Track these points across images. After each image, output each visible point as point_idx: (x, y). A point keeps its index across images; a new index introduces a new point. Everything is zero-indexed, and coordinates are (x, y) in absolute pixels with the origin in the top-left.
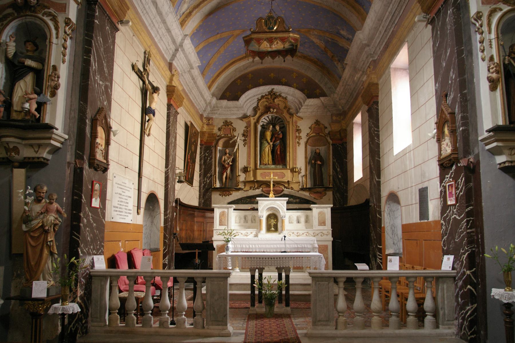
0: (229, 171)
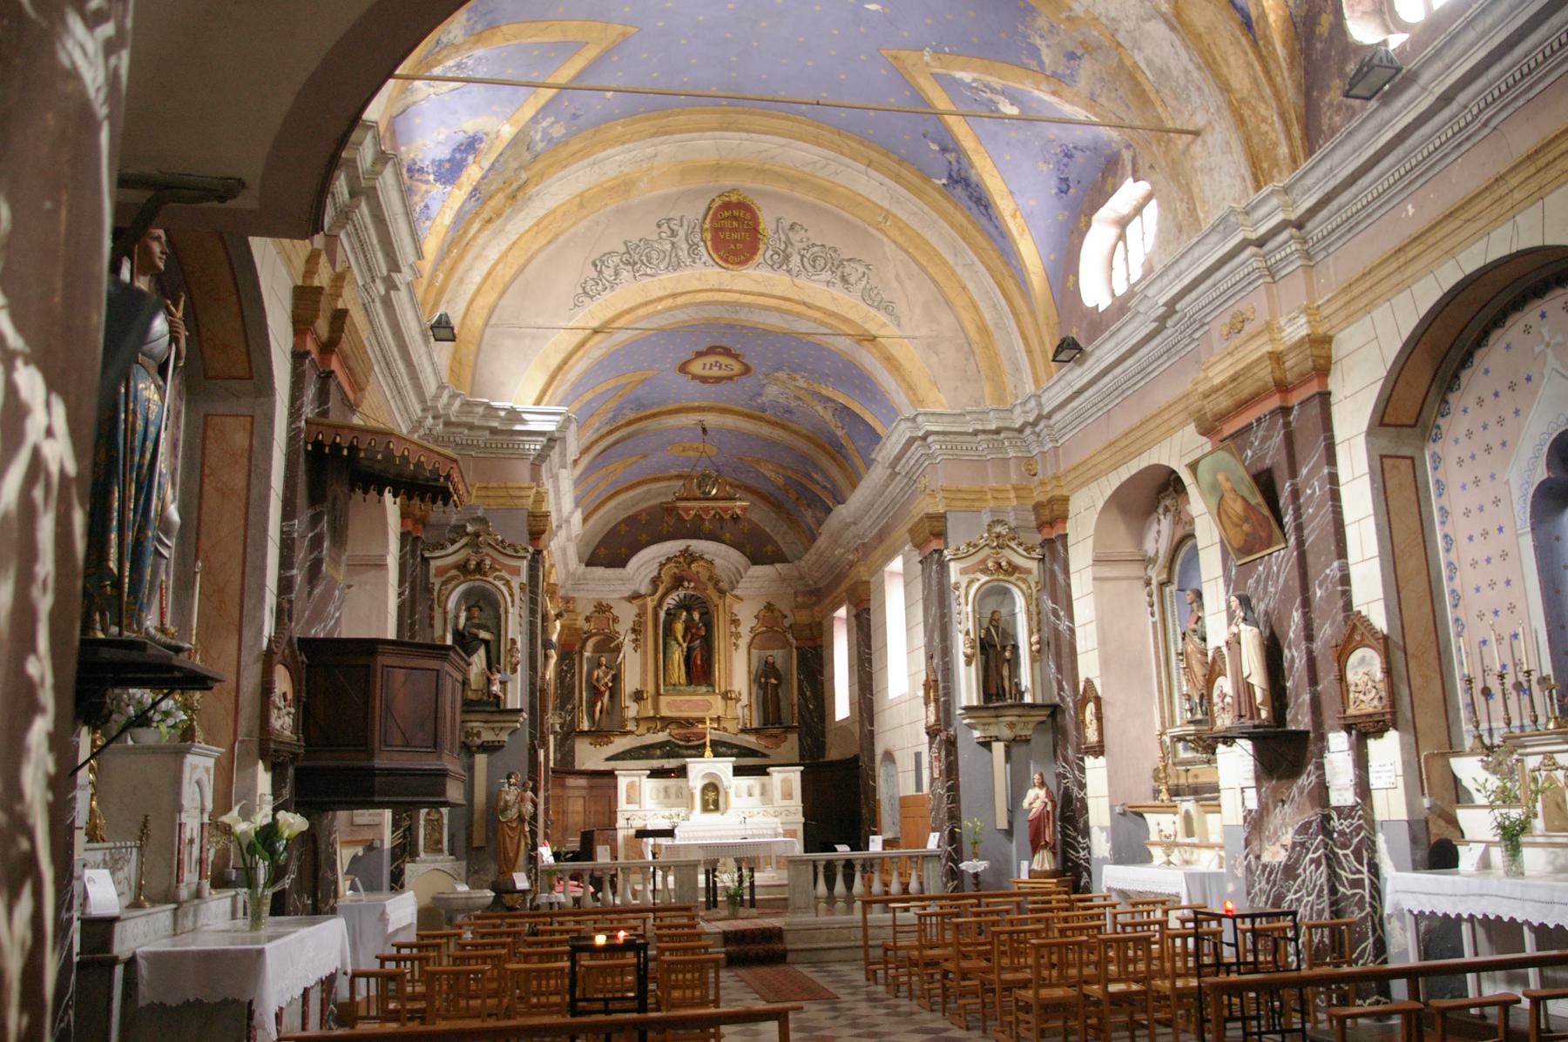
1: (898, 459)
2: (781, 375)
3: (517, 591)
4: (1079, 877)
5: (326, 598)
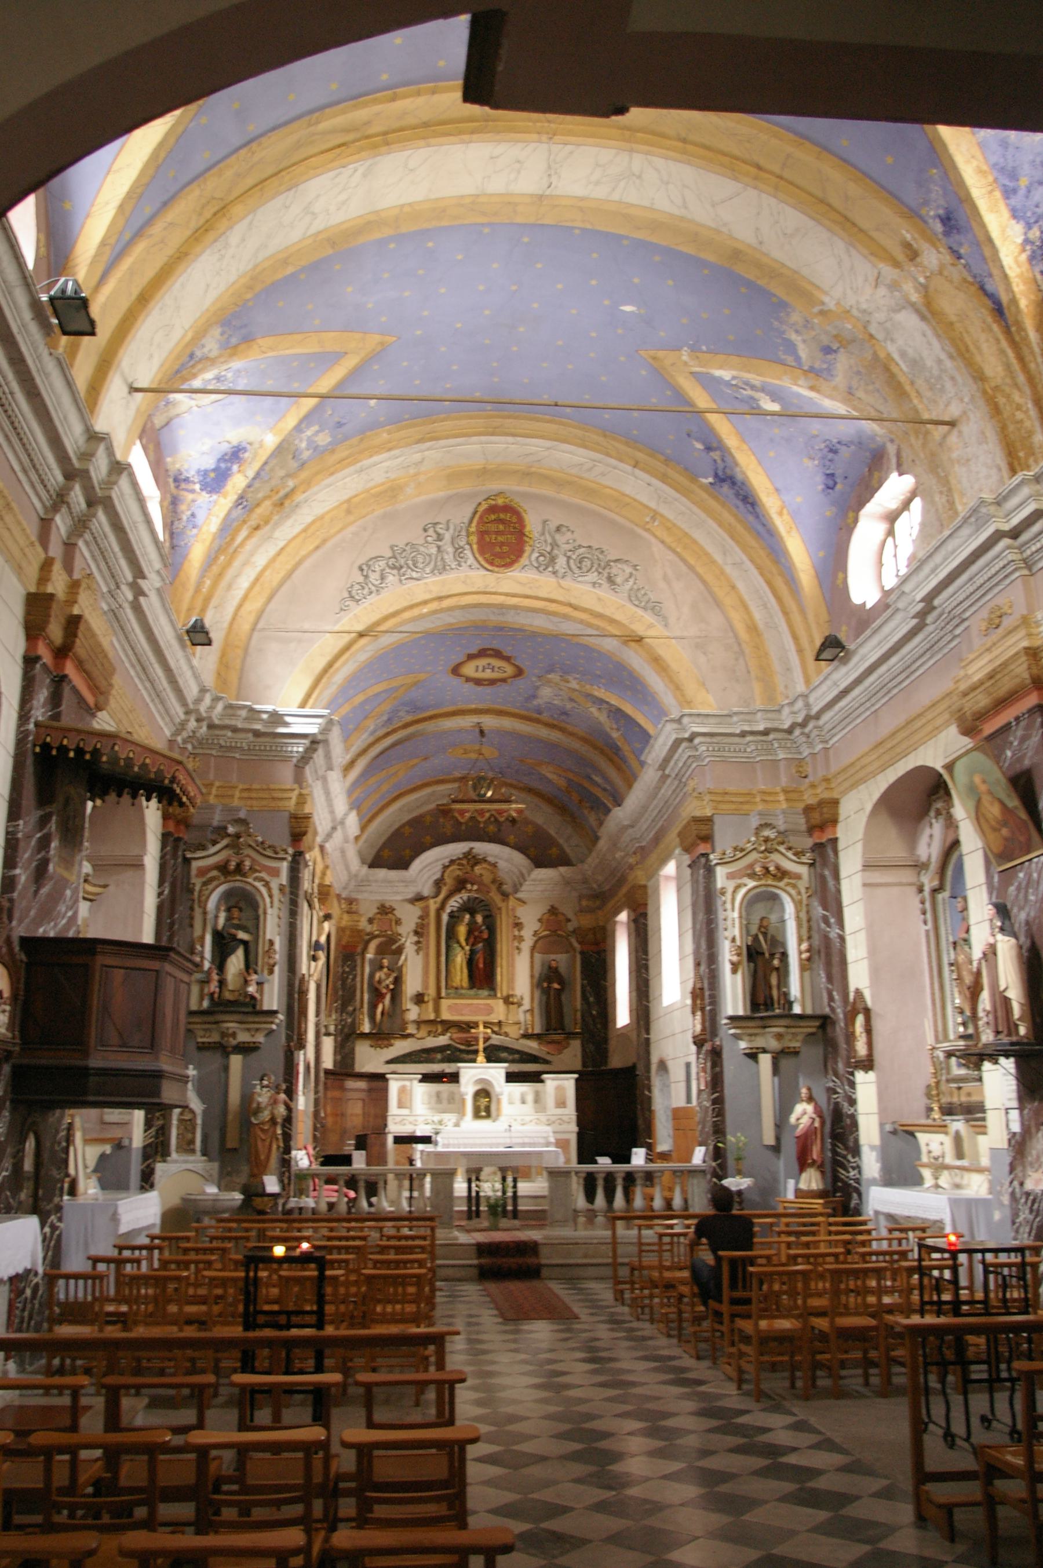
0: (387, 1000)
1: (666, 760)
2: (554, 677)
3: (276, 892)
4: (849, 1197)
5: (56, 897)
